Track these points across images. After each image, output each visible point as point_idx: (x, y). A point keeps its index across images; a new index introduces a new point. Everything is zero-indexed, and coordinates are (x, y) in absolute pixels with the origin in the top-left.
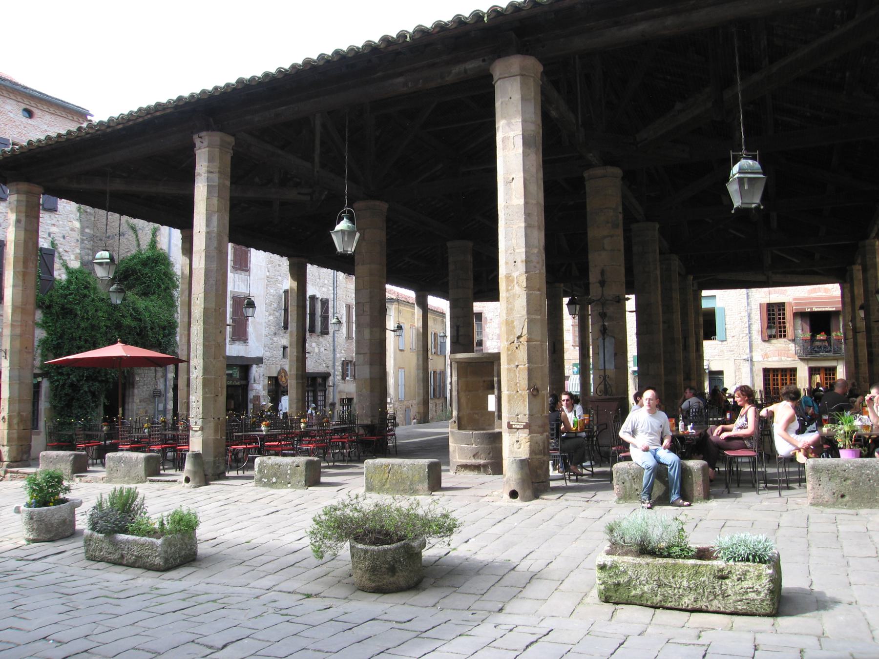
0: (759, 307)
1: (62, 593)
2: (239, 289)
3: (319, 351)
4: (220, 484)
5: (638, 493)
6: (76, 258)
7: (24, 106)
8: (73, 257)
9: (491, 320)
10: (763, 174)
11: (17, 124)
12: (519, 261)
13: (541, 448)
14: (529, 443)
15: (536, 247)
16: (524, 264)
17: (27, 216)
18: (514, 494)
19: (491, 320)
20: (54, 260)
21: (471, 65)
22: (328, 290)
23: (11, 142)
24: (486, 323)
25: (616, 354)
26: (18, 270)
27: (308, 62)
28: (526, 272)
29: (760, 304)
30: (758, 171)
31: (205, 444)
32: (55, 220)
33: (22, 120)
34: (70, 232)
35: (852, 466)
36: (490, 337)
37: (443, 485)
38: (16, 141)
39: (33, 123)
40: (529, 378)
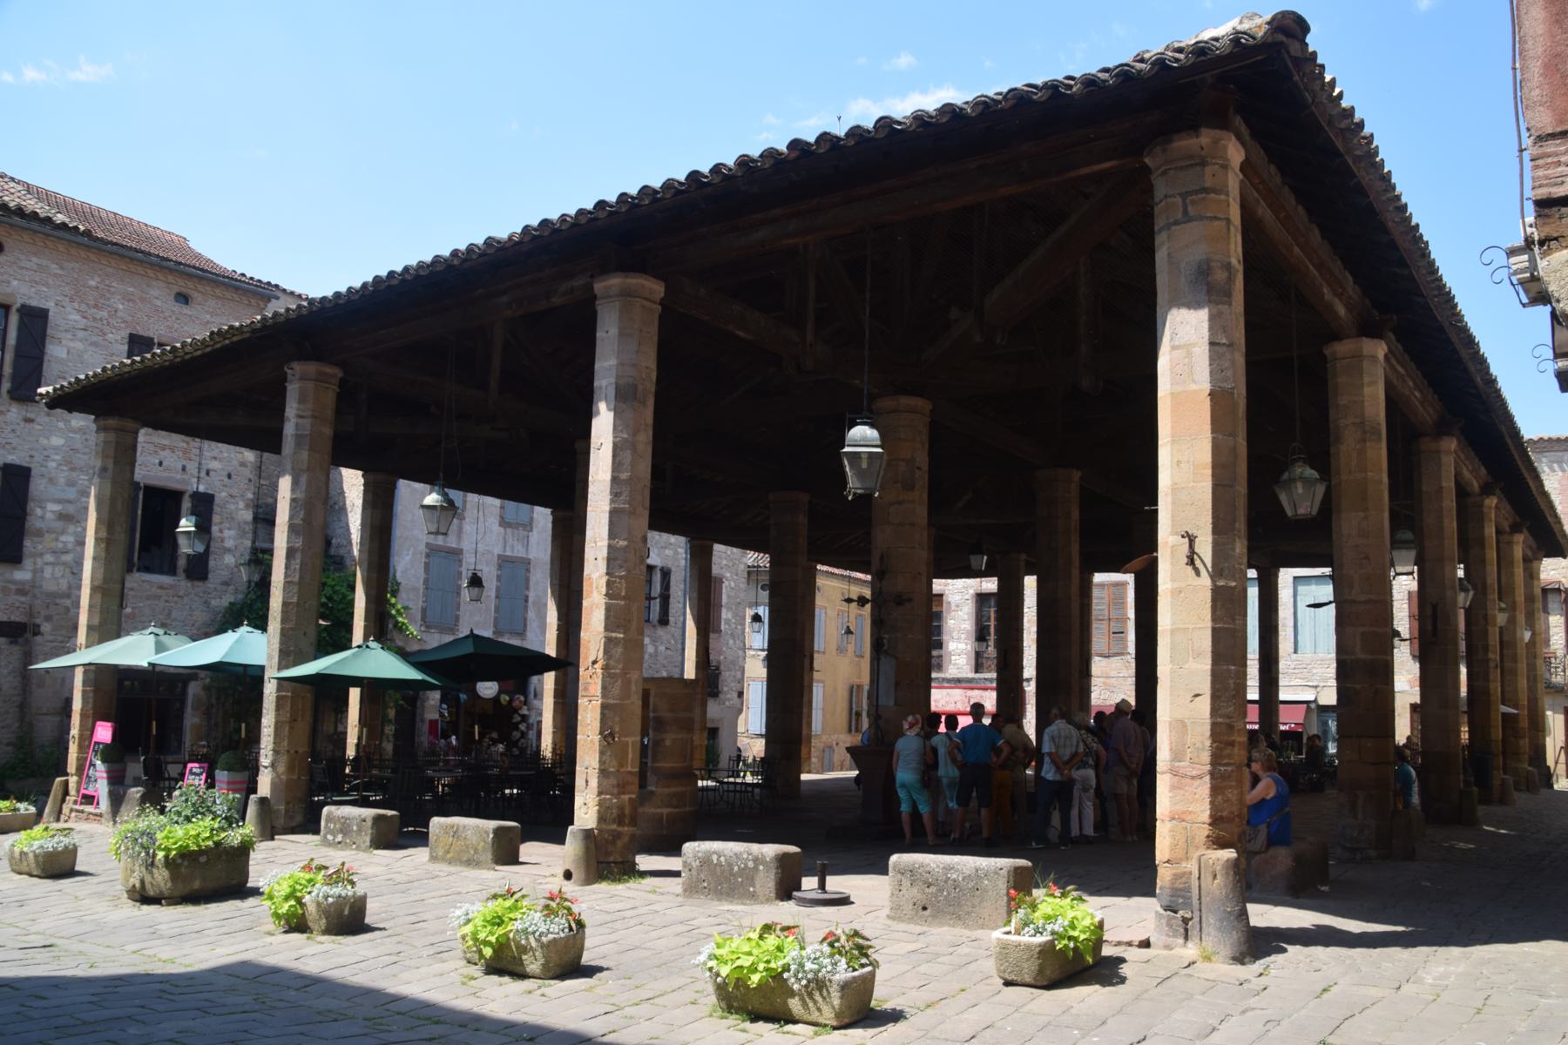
0: (1406, 597)
1: (419, 1018)
2: (513, 551)
3: (656, 651)
4: (285, 840)
5: (705, 885)
6: (247, 506)
7: (176, 289)
8: (241, 505)
9: (957, 606)
11: (166, 314)
12: (600, 558)
14: (597, 808)
16: (605, 562)
17: (115, 463)
18: (568, 875)
19: (957, 606)
20: (212, 510)
21: (578, 282)
22: (676, 553)
23: (156, 341)
24: (949, 611)
25: (897, 684)
26: (100, 535)
27: (437, 260)
28: (607, 574)
29: (1409, 592)
30: (874, 443)
31: (274, 786)
32: (217, 451)
33: (174, 309)
34: (239, 468)
35: (938, 866)
36: (955, 635)
37: (521, 860)
38: (164, 340)
39: (190, 313)
40: (602, 719)
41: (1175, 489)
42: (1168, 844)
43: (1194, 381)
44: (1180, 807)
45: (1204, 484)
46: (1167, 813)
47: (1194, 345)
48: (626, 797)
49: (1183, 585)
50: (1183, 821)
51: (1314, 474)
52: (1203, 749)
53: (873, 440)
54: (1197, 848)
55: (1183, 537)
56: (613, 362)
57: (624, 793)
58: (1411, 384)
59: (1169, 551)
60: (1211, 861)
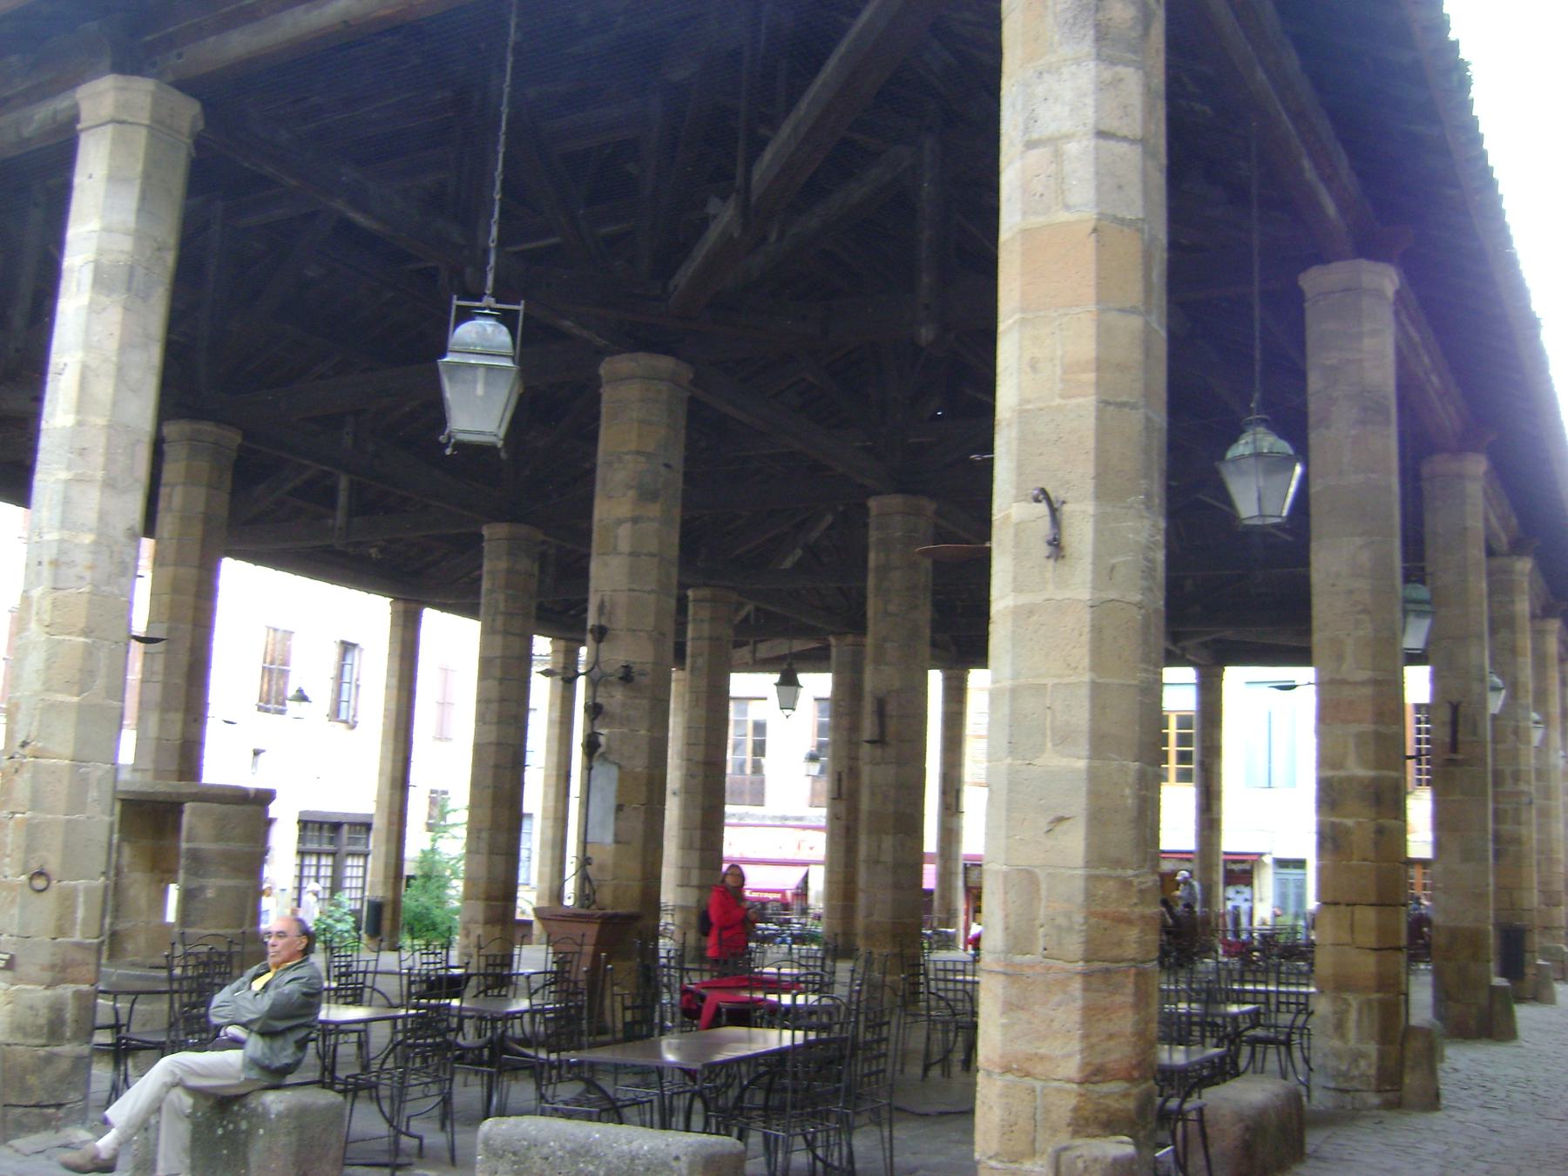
10: (513, 358)
13: (42, 1021)
15: (91, 530)
25: (619, 808)
30: (503, 351)
35: (562, 1147)
41: (1023, 414)
42: (997, 1119)
43: (1067, 207)
44: (1023, 1047)
45: (1080, 400)
46: (996, 1058)
47: (1068, 137)
48: (67, 990)
49: (1038, 598)
50: (1027, 1074)
51: (1284, 447)
52: (1070, 929)
53: (501, 347)
54: (1055, 1131)
55: (1037, 500)
56: (95, 225)
57: (63, 981)
58: (1426, 360)
59: (1011, 531)
60: (1080, 1165)
